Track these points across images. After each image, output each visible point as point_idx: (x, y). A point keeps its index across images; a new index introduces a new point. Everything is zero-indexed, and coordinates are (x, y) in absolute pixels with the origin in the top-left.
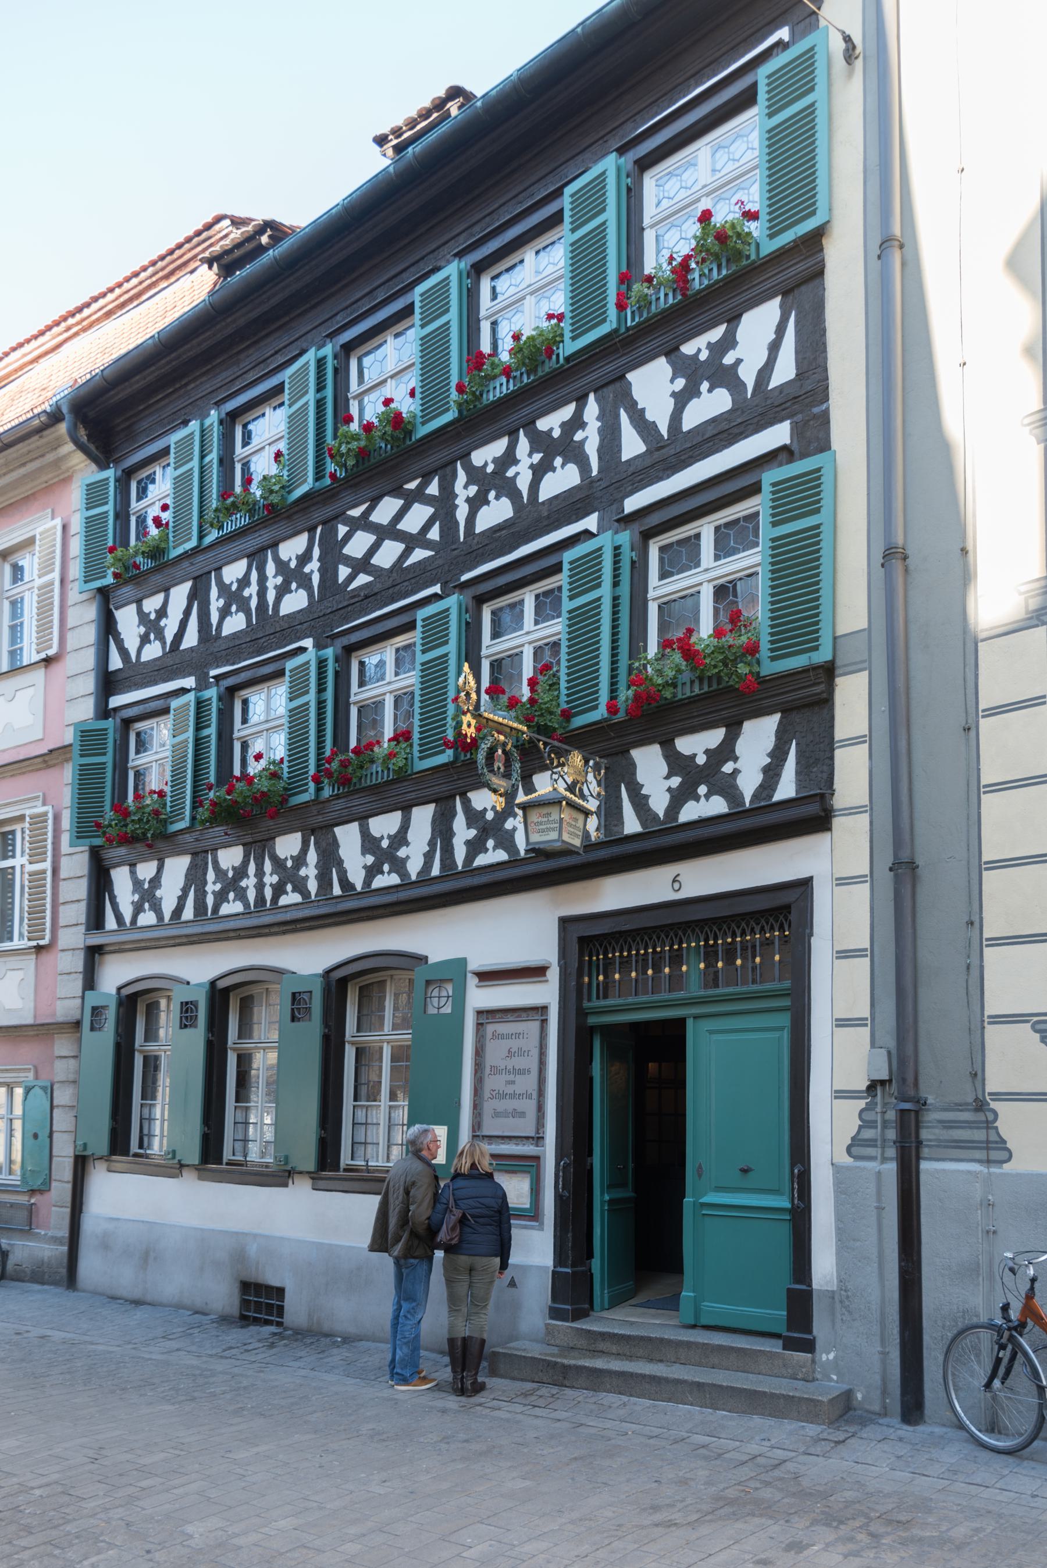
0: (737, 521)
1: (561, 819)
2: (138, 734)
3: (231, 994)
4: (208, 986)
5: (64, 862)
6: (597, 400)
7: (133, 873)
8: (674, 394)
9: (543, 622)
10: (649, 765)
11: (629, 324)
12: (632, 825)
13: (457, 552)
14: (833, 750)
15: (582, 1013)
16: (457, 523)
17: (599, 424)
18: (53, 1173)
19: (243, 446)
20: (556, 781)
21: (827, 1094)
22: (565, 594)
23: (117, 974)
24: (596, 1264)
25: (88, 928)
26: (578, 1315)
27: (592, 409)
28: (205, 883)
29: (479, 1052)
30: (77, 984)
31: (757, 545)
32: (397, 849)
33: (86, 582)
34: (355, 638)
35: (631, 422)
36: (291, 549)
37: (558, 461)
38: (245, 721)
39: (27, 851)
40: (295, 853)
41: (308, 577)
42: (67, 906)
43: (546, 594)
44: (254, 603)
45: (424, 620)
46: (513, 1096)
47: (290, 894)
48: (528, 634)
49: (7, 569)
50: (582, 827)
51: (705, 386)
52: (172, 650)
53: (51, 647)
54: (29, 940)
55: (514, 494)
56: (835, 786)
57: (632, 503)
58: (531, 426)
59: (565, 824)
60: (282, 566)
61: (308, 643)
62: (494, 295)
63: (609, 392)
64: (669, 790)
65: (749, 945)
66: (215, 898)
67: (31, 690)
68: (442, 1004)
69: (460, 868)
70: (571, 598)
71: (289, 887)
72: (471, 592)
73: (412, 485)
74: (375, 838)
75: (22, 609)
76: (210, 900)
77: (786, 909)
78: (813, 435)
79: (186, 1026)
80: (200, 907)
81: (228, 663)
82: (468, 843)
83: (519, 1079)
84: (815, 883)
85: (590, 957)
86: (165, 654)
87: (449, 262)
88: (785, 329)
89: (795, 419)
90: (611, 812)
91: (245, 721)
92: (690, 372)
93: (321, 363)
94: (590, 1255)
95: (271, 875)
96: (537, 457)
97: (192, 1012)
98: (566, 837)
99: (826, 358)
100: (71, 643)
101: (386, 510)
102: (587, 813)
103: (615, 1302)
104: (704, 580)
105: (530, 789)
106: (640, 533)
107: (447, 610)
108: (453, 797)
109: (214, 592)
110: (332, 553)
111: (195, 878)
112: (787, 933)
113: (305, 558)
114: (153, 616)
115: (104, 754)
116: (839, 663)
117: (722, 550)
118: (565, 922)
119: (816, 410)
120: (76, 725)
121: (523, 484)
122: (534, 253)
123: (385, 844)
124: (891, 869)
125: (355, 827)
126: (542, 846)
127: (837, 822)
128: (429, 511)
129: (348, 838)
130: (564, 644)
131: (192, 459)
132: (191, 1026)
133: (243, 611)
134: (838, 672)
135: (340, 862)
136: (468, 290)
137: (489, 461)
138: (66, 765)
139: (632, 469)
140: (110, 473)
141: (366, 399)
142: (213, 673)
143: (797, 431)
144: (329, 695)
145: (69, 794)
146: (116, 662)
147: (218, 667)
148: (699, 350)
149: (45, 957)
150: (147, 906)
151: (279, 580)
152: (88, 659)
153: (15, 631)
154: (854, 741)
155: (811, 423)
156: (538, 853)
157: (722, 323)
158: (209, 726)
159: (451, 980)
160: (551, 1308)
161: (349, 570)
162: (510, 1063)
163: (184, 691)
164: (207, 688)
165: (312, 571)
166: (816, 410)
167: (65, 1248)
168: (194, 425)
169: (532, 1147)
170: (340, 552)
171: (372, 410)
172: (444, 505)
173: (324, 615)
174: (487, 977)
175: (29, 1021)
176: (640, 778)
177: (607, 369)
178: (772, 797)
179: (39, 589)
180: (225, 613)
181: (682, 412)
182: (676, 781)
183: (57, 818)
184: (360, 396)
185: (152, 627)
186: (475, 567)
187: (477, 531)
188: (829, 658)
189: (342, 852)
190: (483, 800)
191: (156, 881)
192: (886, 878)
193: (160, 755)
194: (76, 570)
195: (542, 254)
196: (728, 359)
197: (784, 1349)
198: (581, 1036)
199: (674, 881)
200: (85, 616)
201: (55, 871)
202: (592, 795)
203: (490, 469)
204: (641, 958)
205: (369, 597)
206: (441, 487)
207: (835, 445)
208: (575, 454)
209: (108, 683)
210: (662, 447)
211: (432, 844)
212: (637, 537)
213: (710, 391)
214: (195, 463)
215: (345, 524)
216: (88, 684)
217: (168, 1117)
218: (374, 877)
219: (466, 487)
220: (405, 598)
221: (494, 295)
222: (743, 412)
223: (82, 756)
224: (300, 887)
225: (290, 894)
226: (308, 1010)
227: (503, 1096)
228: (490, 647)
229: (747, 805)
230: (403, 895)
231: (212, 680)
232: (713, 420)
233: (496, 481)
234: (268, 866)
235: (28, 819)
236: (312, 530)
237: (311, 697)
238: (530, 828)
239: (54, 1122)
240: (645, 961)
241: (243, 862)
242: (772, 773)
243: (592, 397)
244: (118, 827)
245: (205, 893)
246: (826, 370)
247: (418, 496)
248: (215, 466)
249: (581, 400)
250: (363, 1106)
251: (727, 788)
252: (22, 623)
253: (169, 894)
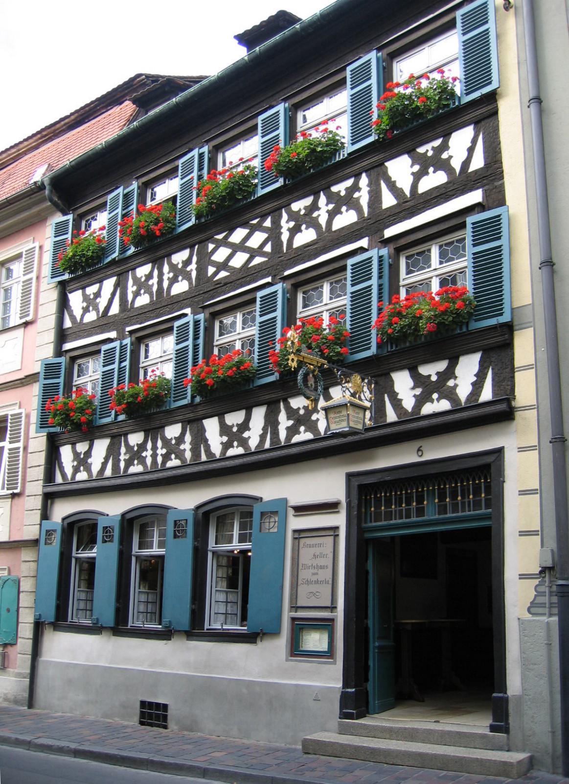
1: (348, 415)
2: (79, 366)
3: (135, 522)
4: (120, 518)
8: (413, 174)
10: (403, 383)
12: (391, 416)
13: (280, 259)
15: (361, 531)
16: (282, 242)
17: (368, 189)
19: (152, 201)
20: (344, 391)
23: (62, 510)
24: (370, 686)
27: (364, 181)
28: (120, 454)
30: (37, 516)
31: (465, 256)
32: (243, 433)
33: (52, 278)
35: (388, 188)
37: (344, 209)
38: (146, 357)
41: (189, 273)
42: (31, 469)
44: (155, 288)
48: (327, 305)
49: (4, 271)
51: (431, 170)
52: (103, 316)
53: (28, 315)
56: (516, 394)
57: (389, 233)
58: (328, 190)
61: (188, 311)
63: (373, 173)
65: (466, 488)
68: (271, 526)
71: (173, 456)
72: (293, 281)
76: (122, 465)
78: (496, 197)
80: (116, 467)
82: (288, 428)
83: (320, 571)
84: (506, 450)
86: (98, 319)
88: (477, 141)
91: (146, 357)
93: (201, 156)
97: (110, 532)
98: (352, 424)
99: (501, 157)
101: (238, 235)
102: (364, 409)
103: (385, 708)
104: (435, 273)
105: (328, 397)
106: (394, 249)
108: (278, 402)
110: (204, 260)
111: (112, 452)
113: (188, 262)
114: (92, 297)
116: (515, 323)
119: (497, 184)
121: (323, 220)
123: (235, 429)
127: (518, 415)
128: (265, 236)
130: (348, 311)
132: (109, 541)
134: (515, 328)
135: (206, 441)
136: (290, 117)
138: (34, 384)
139: (388, 213)
140: (70, 217)
142: (128, 329)
143: (486, 195)
144: (201, 341)
149: (16, 500)
150: (82, 468)
152: (52, 322)
153: (6, 305)
155: (494, 190)
157: (440, 137)
159: (276, 512)
165: (192, 270)
170: (210, 258)
172: (274, 234)
176: (397, 388)
178: (478, 400)
180: (137, 294)
181: (418, 183)
182: (418, 391)
188: (509, 320)
189: (208, 435)
190: (298, 403)
191: (88, 454)
192: (548, 448)
193: (91, 377)
196: (445, 156)
199: (419, 450)
200: (49, 297)
201: (25, 448)
202: (366, 400)
203: (302, 212)
204: (398, 497)
205: (226, 284)
207: (508, 203)
208: (353, 204)
209: (62, 336)
210: (406, 202)
211: (265, 429)
212: (392, 251)
213: (434, 172)
215: (213, 243)
216: (51, 336)
219: (287, 222)
223: (45, 379)
224: (180, 455)
226: (184, 532)
228: (302, 312)
230: (88, 485)
234: (159, 443)
237: (190, 343)
238: (330, 421)
239: (20, 601)
240: (401, 499)
242: (478, 386)
244: (68, 422)
245: (119, 460)
247: (259, 227)
249: (357, 176)
251: (450, 395)
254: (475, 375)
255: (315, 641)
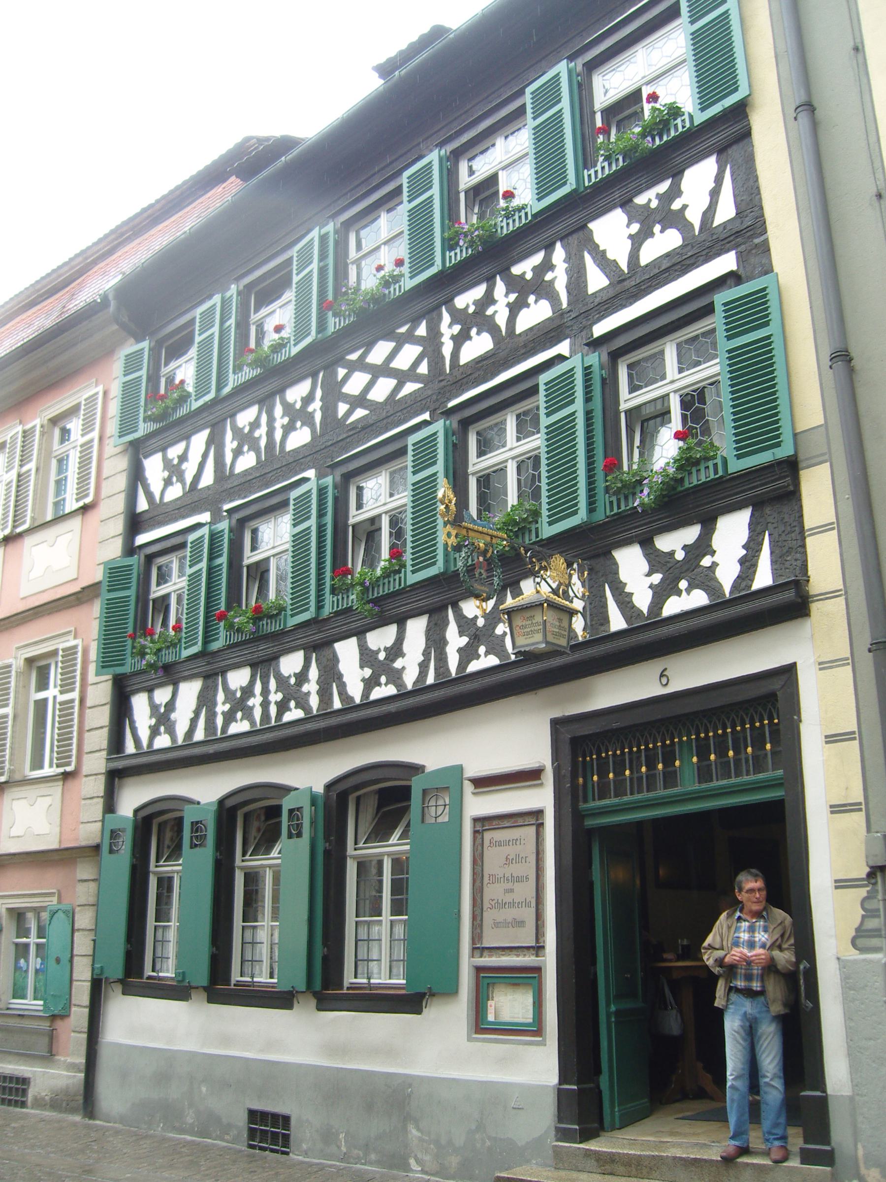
0: (697, 337)
4: (215, 807)
5: (90, 690)
6: (563, 247)
7: (151, 699)
8: (631, 237)
9: (524, 438)
11: (587, 184)
12: (617, 622)
13: (444, 380)
14: (804, 539)
15: (578, 816)
16: (443, 357)
17: (566, 265)
18: (73, 998)
21: (829, 884)
22: (542, 411)
23: (134, 797)
24: (604, 1081)
25: (110, 752)
26: (586, 1135)
27: (559, 254)
28: (215, 704)
29: (478, 860)
30: (98, 806)
31: (715, 357)
32: (393, 661)
33: (120, 437)
34: (352, 466)
36: (296, 394)
37: (532, 299)
39: (59, 682)
40: (298, 670)
41: (311, 415)
43: (525, 413)
44: (263, 443)
45: (414, 445)
46: (512, 904)
47: (294, 710)
50: (567, 626)
51: (657, 228)
54: (57, 766)
55: (493, 329)
56: (809, 573)
57: (600, 329)
59: (548, 624)
60: (288, 408)
61: (311, 473)
62: (471, 172)
63: (573, 240)
64: (651, 587)
66: (224, 718)
67: (69, 536)
68: (439, 813)
69: (454, 675)
70: (548, 415)
73: (403, 330)
74: (373, 651)
75: (67, 465)
76: (219, 721)
77: (771, 697)
79: (196, 845)
81: (240, 498)
82: (460, 650)
83: (517, 887)
85: (584, 758)
86: (185, 494)
87: (431, 151)
89: (739, 249)
90: (596, 613)
92: (643, 218)
93: (323, 239)
94: (598, 1071)
95: (275, 693)
96: (513, 297)
100: (105, 491)
101: (379, 353)
102: (572, 613)
105: (518, 592)
107: (435, 434)
108: (444, 608)
109: (229, 435)
110: (333, 393)
111: (206, 700)
112: (776, 721)
113: (308, 400)
114: (176, 462)
115: (129, 588)
116: (801, 457)
117: (522, 432)
118: (556, 724)
120: (105, 564)
122: (503, 138)
123: (382, 656)
124: (870, 651)
125: (353, 641)
126: (527, 649)
128: (418, 349)
129: (347, 651)
131: (213, 326)
133: (254, 450)
134: (801, 465)
135: (340, 676)
137: (470, 304)
139: (597, 300)
140: (145, 345)
141: (363, 263)
142: (227, 507)
143: (740, 258)
145: (97, 628)
146: (142, 505)
147: (231, 501)
148: (650, 200)
149: (70, 784)
150: (162, 729)
151: (286, 420)
152: (118, 505)
154: (824, 529)
155: (754, 251)
156: (526, 657)
158: (221, 555)
160: (557, 1129)
161: (348, 406)
162: (509, 871)
163: (199, 526)
164: (220, 521)
165: (315, 410)
166: (756, 241)
167: (82, 1075)
168: (217, 299)
169: (533, 958)
171: (370, 282)
173: (326, 447)
174: (484, 783)
175: (54, 845)
176: (623, 576)
177: (571, 221)
178: (751, 586)
179: (81, 446)
180: (237, 453)
181: (639, 251)
183: (86, 652)
184: (358, 262)
185: (174, 471)
186: (460, 395)
187: (462, 363)
188: (792, 453)
189: (342, 667)
191: (171, 705)
194: (113, 427)
195: (510, 138)
196: (676, 205)
197: (802, 1163)
198: (583, 843)
199: (662, 675)
200: (117, 467)
201: (82, 700)
202: (576, 596)
203: (471, 309)
205: (365, 429)
206: (429, 329)
207: (776, 269)
209: (135, 523)
210: (624, 280)
211: (426, 653)
213: (662, 231)
214: (216, 329)
215: (343, 367)
216: (118, 526)
217: (173, 945)
218: (373, 688)
219: (450, 326)
220: (398, 426)
221: (471, 172)
222: (693, 247)
224: (302, 704)
225: (294, 710)
227: (502, 905)
229: (728, 595)
230: (392, 707)
231: (225, 514)
232: (667, 255)
233: (479, 318)
235: (61, 653)
236: (314, 375)
237: (312, 522)
238: (515, 632)
239: (75, 946)
241: (250, 682)
242: (748, 564)
243: (558, 245)
245: (214, 714)
246: (762, 208)
247: (410, 338)
248: (233, 330)
249: (549, 248)
250: (366, 921)
251: (706, 580)
252: (66, 477)
253: (182, 718)
254: (744, 547)
255: (511, 1005)
